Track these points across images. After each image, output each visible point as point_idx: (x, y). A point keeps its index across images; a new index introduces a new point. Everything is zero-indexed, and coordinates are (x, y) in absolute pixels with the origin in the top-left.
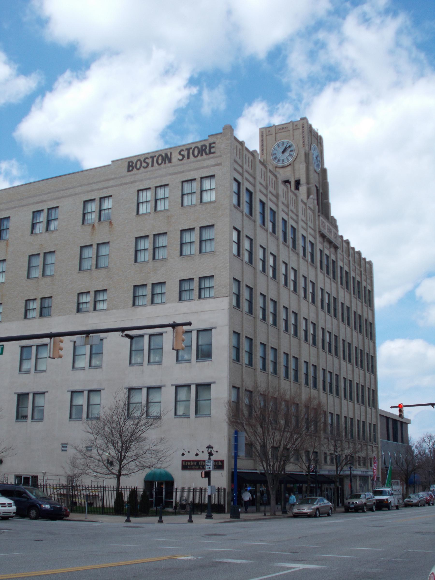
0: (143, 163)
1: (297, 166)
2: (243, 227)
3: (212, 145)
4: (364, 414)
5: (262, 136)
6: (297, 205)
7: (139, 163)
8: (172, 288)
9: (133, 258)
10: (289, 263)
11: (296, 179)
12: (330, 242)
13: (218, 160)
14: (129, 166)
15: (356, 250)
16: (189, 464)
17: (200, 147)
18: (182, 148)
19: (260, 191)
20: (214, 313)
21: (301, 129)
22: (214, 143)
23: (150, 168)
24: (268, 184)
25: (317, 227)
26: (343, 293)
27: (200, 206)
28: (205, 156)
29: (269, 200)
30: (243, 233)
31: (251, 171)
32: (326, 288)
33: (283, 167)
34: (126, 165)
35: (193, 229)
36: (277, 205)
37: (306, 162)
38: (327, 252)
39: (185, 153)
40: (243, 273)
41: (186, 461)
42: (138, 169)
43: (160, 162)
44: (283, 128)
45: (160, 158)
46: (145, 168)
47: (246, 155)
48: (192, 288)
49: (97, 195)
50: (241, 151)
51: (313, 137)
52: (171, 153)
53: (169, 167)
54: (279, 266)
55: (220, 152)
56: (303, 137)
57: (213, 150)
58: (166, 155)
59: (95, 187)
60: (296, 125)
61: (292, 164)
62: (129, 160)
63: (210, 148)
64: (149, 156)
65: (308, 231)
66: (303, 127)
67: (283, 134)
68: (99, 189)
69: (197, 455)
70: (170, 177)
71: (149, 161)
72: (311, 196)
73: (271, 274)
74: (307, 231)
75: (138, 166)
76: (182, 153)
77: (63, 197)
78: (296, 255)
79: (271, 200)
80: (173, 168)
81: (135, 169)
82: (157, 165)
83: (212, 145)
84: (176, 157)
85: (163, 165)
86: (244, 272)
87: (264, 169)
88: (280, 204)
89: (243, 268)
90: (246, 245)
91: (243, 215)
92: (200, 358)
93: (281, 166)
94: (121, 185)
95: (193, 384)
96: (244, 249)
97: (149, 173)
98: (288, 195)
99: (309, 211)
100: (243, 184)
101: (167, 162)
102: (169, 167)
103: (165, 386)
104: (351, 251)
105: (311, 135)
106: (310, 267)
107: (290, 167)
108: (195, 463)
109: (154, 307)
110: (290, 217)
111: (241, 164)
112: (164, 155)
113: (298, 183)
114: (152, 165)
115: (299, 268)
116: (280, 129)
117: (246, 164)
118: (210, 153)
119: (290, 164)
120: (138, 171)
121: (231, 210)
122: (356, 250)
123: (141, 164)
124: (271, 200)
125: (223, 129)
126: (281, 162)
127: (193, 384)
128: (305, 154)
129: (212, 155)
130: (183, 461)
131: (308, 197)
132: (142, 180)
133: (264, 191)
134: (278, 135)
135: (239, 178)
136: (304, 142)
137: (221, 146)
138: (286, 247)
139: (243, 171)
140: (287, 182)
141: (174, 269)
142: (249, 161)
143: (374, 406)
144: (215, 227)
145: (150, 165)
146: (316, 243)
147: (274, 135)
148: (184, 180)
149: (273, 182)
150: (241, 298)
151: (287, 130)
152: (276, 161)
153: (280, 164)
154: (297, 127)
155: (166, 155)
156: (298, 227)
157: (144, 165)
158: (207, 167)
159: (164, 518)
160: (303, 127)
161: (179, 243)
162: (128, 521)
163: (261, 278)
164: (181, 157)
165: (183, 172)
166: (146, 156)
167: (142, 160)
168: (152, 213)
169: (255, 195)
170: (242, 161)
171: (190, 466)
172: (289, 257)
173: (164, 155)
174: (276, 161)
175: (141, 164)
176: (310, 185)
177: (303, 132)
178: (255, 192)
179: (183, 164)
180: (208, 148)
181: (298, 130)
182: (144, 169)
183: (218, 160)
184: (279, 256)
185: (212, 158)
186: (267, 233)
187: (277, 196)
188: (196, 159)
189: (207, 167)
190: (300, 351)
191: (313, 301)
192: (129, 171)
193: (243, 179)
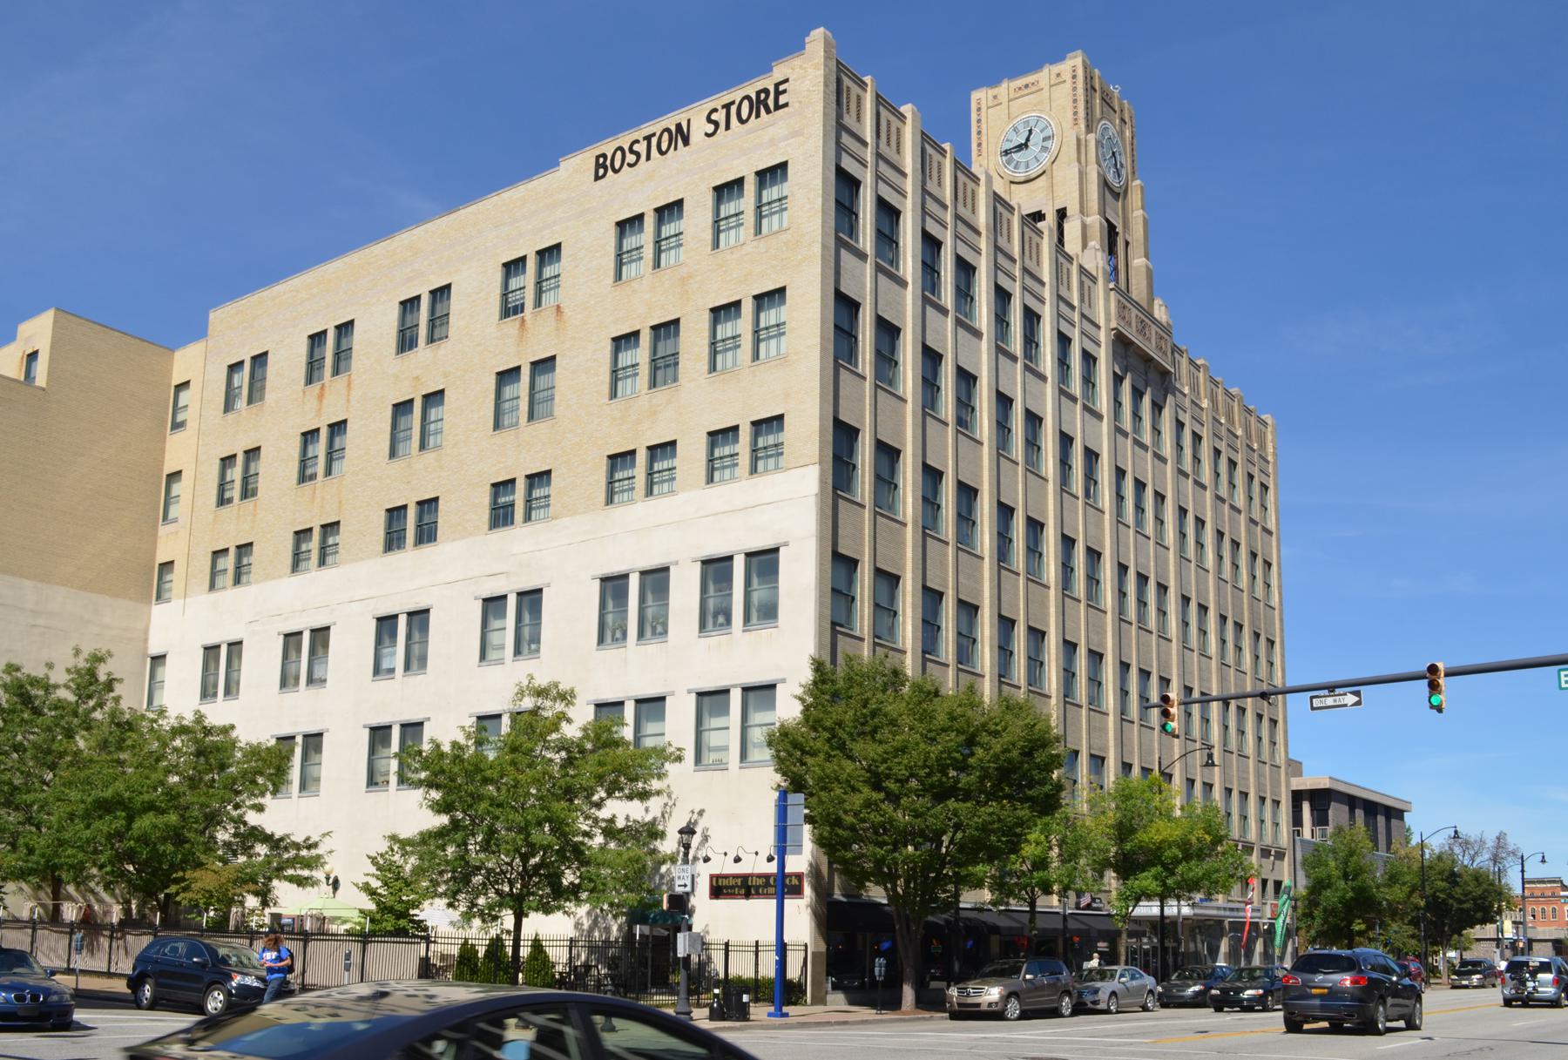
3: (781, 88)
8: (692, 453)
16: (725, 882)
20: (782, 506)
21: (1069, 81)
22: (786, 81)
41: (718, 877)
43: (664, 147)
63: (778, 93)
66: (1074, 77)
69: (737, 860)
81: (610, 172)
83: (781, 88)
92: (754, 619)
103: (673, 694)
108: (739, 881)
113: (1062, 214)
114: (648, 158)
118: (778, 107)
126: (1022, 166)
127: (735, 686)
130: (712, 877)
131: (1085, 246)
147: (1004, 106)
153: (1021, 176)
157: (631, 158)
160: (1074, 77)
167: (626, 148)
171: (727, 887)
173: (673, 129)
192: (597, 178)
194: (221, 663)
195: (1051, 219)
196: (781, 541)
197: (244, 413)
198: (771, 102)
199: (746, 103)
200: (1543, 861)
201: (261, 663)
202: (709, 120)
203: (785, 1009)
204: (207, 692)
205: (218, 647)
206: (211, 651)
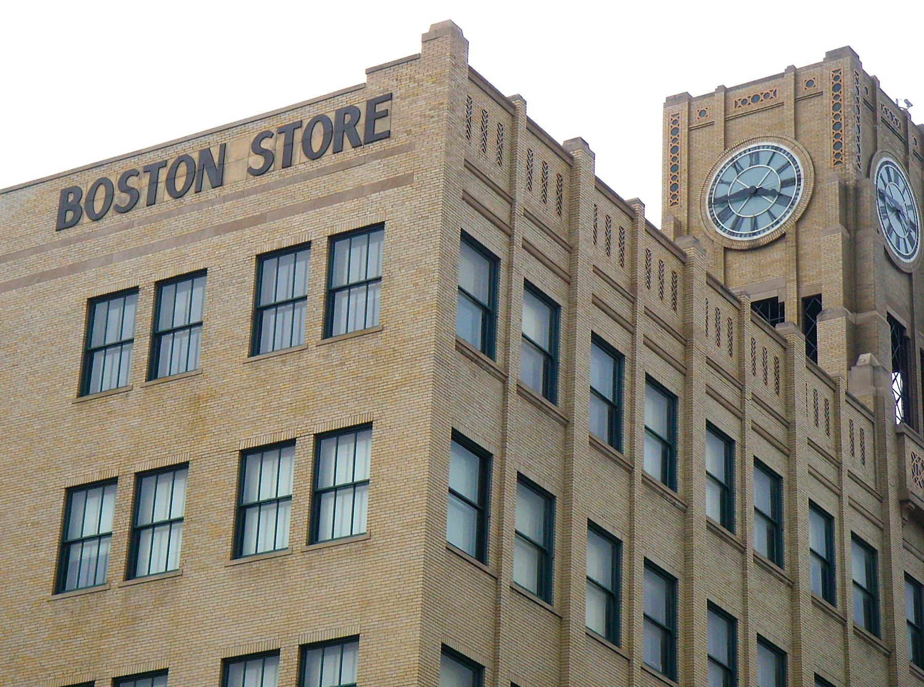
0: (117, 192)
1: (809, 240)
2: (504, 440)
3: (380, 108)
5: (675, 131)
6: (790, 382)
7: (101, 192)
10: (745, 614)
11: (806, 293)
13: (399, 165)
14: (64, 207)
17: (332, 116)
18: (263, 126)
19: (598, 303)
23: (142, 211)
25: (892, 481)
27: (323, 350)
28: (349, 152)
30: (746, 628)
31: (551, 218)
33: (755, 248)
34: (54, 201)
35: (291, 443)
36: (685, 373)
37: (845, 222)
40: (497, 634)
42: (97, 218)
44: (755, 98)
45: (183, 169)
50: (506, 134)
51: (881, 128)
52: (223, 147)
53: (211, 203)
55: (409, 133)
56: (837, 126)
57: (380, 127)
58: (206, 154)
60: (810, 83)
61: (791, 237)
62: (64, 184)
63: (373, 116)
64: (138, 164)
65: (845, 493)
66: (836, 87)
67: (754, 118)
70: (216, 239)
71: (141, 183)
72: (865, 358)
75: (98, 207)
76: (266, 144)
78: (783, 587)
80: (228, 204)
81: (85, 219)
82: (167, 197)
83: (380, 108)
84: (241, 158)
85: (190, 197)
86: (503, 630)
88: (698, 367)
89: (497, 610)
90: (518, 516)
91: (505, 390)
93: (745, 246)
94: (30, 281)
96: (508, 533)
97: (135, 230)
98: (741, 336)
99: (847, 412)
100: (510, 266)
101: (206, 182)
102: (211, 203)
105: (875, 118)
106: (856, 649)
107: (780, 246)
110: (748, 424)
111: (503, 184)
112: (195, 156)
113: (812, 307)
114: (151, 202)
115: (796, 644)
116: (744, 102)
117: (862, 430)
118: (372, 137)
119: (783, 236)
120: (95, 224)
121: (440, 361)
123: (110, 196)
125: (424, 42)
126: (746, 228)
128: (844, 190)
129: (376, 147)
131: (853, 361)
132: (109, 260)
133: (620, 306)
135: (493, 241)
136: (837, 145)
137: (419, 115)
138: (728, 549)
139: (512, 214)
140: (770, 310)
142: (544, 179)
144: (375, 430)
145: (143, 200)
146: (887, 550)
148: (267, 249)
149: (668, 277)
151: (771, 103)
152: (727, 226)
153: (743, 238)
154: (812, 90)
155: (206, 154)
156: (792, 472)
157: (121, 198)
158: (359, 192)
161: (232, 504)
164: (258, 162)
166: (131, 164)
167: (115, 180)
168: (137, 388)
169: (573, 316)
170: (512, 173)
172: (744, 591)
173: (195, 156)
174: (727, 226)
175: (110, 196)
176: (862, 317)
177: (836, 107)
178: (572, 304)
179: (265, 188)
180: (362, 120)
181: (815, 101)
182: (118, 217)
183: (399, 165)
184: (689, 579)
185: (378, 156)
186: (631, 478)
187: (685, 338)
188: (317, 164)
189: (359, 192)
192: (62, 225)
193: (511, 243)
195: (792, 312)
198: (360, 129)
199: (319, 127)
202: (256, 148)
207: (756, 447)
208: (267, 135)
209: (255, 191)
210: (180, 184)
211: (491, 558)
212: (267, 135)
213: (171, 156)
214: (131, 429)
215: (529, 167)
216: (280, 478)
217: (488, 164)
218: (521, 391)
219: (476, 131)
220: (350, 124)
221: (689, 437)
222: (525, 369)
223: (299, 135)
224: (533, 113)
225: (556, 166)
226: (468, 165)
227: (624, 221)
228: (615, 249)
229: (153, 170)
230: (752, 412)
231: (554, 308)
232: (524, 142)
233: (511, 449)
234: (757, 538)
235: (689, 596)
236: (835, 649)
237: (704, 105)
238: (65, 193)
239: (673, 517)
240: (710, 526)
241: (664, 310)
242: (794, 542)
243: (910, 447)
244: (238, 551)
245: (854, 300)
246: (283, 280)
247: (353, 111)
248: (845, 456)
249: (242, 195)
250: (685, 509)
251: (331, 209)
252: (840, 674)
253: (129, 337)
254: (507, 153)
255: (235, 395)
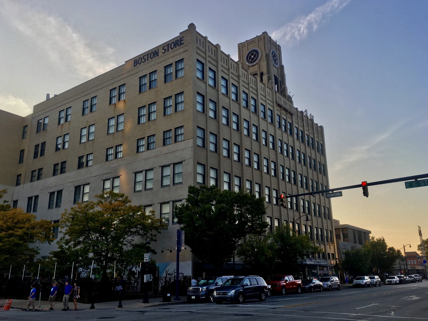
1: (261, 64)
4: (321, 223)
9: (137, 122)
12: (286, 110)
13: (186, 48)
14: (135, 63)
15: (319, 125)
23: (146, 62)
24: (250, 82)
26: (299, 144)
29: (230, 78)
31: (213, 56)
32: (277, 136)
38: (283, 116)
39: (166, 48)
40: (207, 124)
42: (140, 64)
46: (143, 62)
47: (224, 57)
48: (171, 136)
49: (117, 85)
50: (204, 43)
54: (241, 122)
57: (182, 42)
58: (156, 51)
59: (116, 80)
63: (181, 41)
64: (145, 54)
68: (118, 81)
71: (146, 57)
73: (285, 154)
74: (206, 60)
76: (165, 48)
77: (99, 90)
79: (269, 104)
84: (161, 51)
87: (246, 73)
88: (241, 81)
89: (207, 120)
95: (171, 201)
99: (267, 89)
100: (206, 65)
104: (314, 126)
109: (149, 151)
111: (204, 51)
113: (262, 74)
114: (148, 60)
115: (259, 125)
118: (181, 44)
122: (319, 125)
123: (141, 60)
124: (269, 104)
129: (182, 46)
131: (268, 82)
132: (142, 70)
134: (249, 47)
135: (203, 61)
140: (255, 75)
141: (161, 124)
143: (329, 219)
144: (184, 93)
146: (274, 110)
150: (206, 141)
155: (156, 51)
157: (143, 60)
159: (95, 305)
161: (163, 107)
162: (93, 307)
163: (280, 156)
165: (165, 60)
167: (142, 57)
169: (218, 73)
170: (206, 49)
175: (141, 60)
178: (218, 71)
183: (186, 48)
184: (241, 115)
185: (182, 47)
187: (238, 77)
188: (173, 50)
189: (180, 54)
190: (262, 179)
191: (305, 164)
192: (135, 66)
194: (33, 202)
195: (259, 75)
196: (154, 166)
197: (42, 133)
200: (410, 247)
201: (43, 201)
202: (163, 49)
203: (179, 297)
204: (28, 210)
205: (54, 192)
206: (30, 199)
207: (251, 95)
208: (165, 46)
209: (163, 56)
210: (152, 57)
211: (205, 112)
212: (165, 46)
213: (150, 52)
214: (148, 97)
215: (209, 48)
216: (171, 102)
217: (201, 47)
218: (252, 112)
219: (198, 42)
220: (177, 43)
221: (240, 93)
222: (252, 108)
223: (170, 46)
224: (209, 39)
225: (214, 49)
226: (197, 47)
227: (227, 58)
228: (225, 62)
229: (148, 55)
230: (268, 101)
231: (237, 87)
232: (230, 61)
233: (208, 95)
234: (269, 120)
235: (241, 118)
236: (266, 126)
237: (244, 44)
238: (135, 61)
239: (238, 105)
240: (262, 118)
241: (235, 72)
242: (258, 109)
243: (277, 94)
244: (165, 114)
245: (269, 72)
246: (169, 71)
247: (178, 40)
248: (267, 96)
249: (161, 57)
250: (258, 116)
251: (175, 57)
252: (266, 129)
253: (146, 83)
254: (204, 45)
255: (165, 90)
